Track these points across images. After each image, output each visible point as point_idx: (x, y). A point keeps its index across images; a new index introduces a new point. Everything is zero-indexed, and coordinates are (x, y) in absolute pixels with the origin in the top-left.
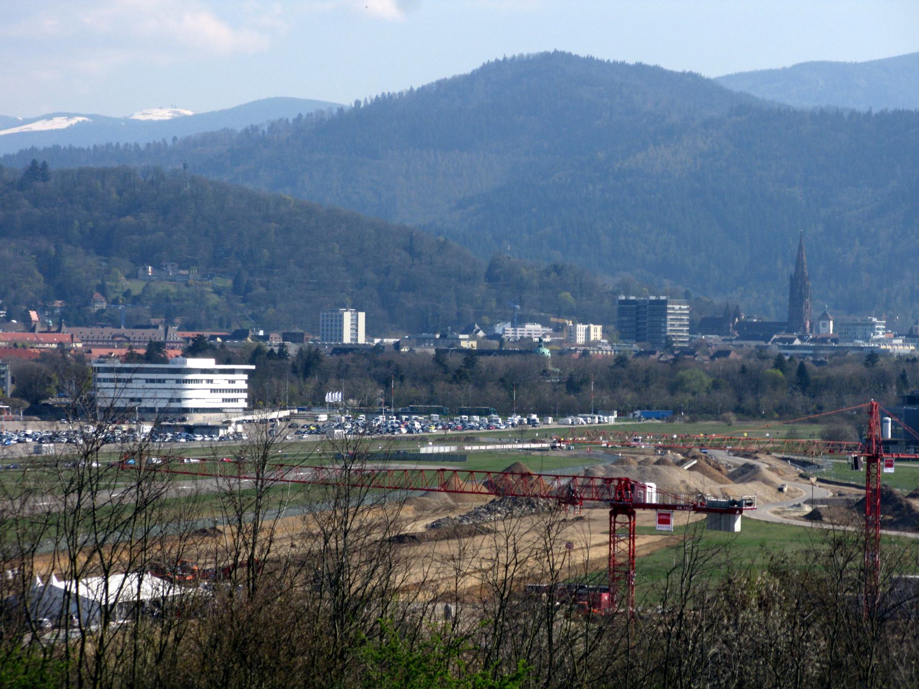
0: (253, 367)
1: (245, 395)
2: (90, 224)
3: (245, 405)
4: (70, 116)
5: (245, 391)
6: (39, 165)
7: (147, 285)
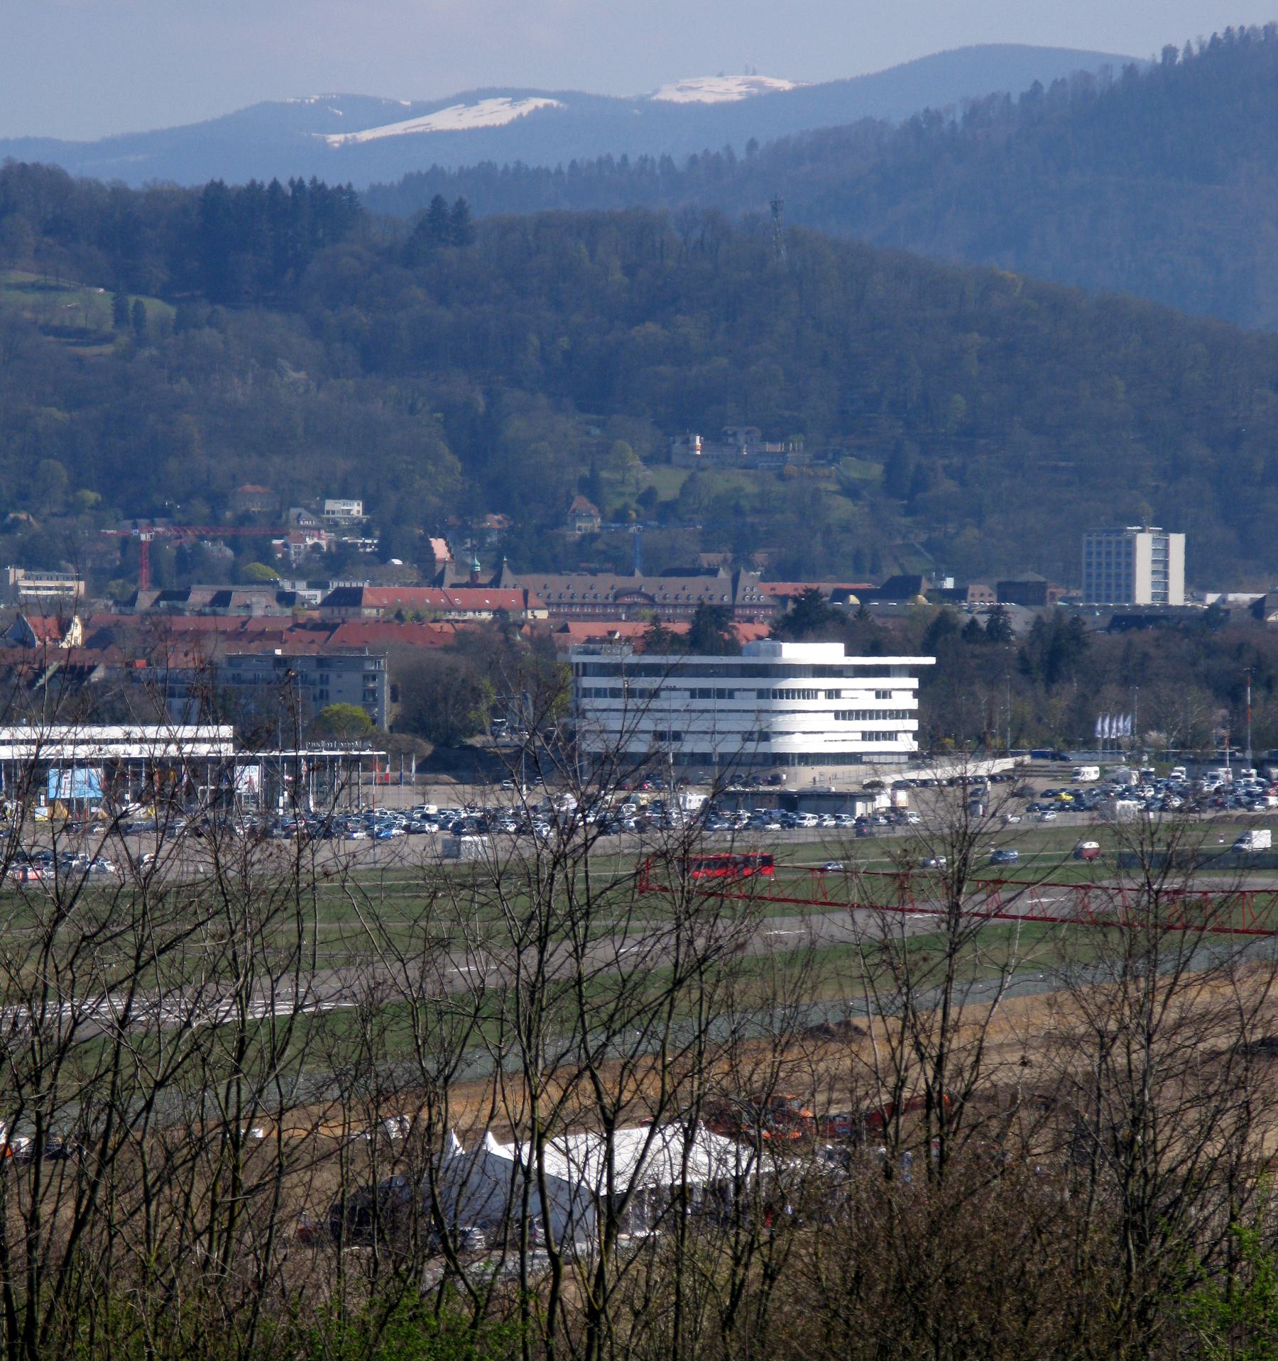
0: (931, 660)
1: (913, 725)
2: (564, 342)
3: (914, 746)
4: (517, 95)
5: (912, 714)
6: (450, 203)
7: (692, 478)
